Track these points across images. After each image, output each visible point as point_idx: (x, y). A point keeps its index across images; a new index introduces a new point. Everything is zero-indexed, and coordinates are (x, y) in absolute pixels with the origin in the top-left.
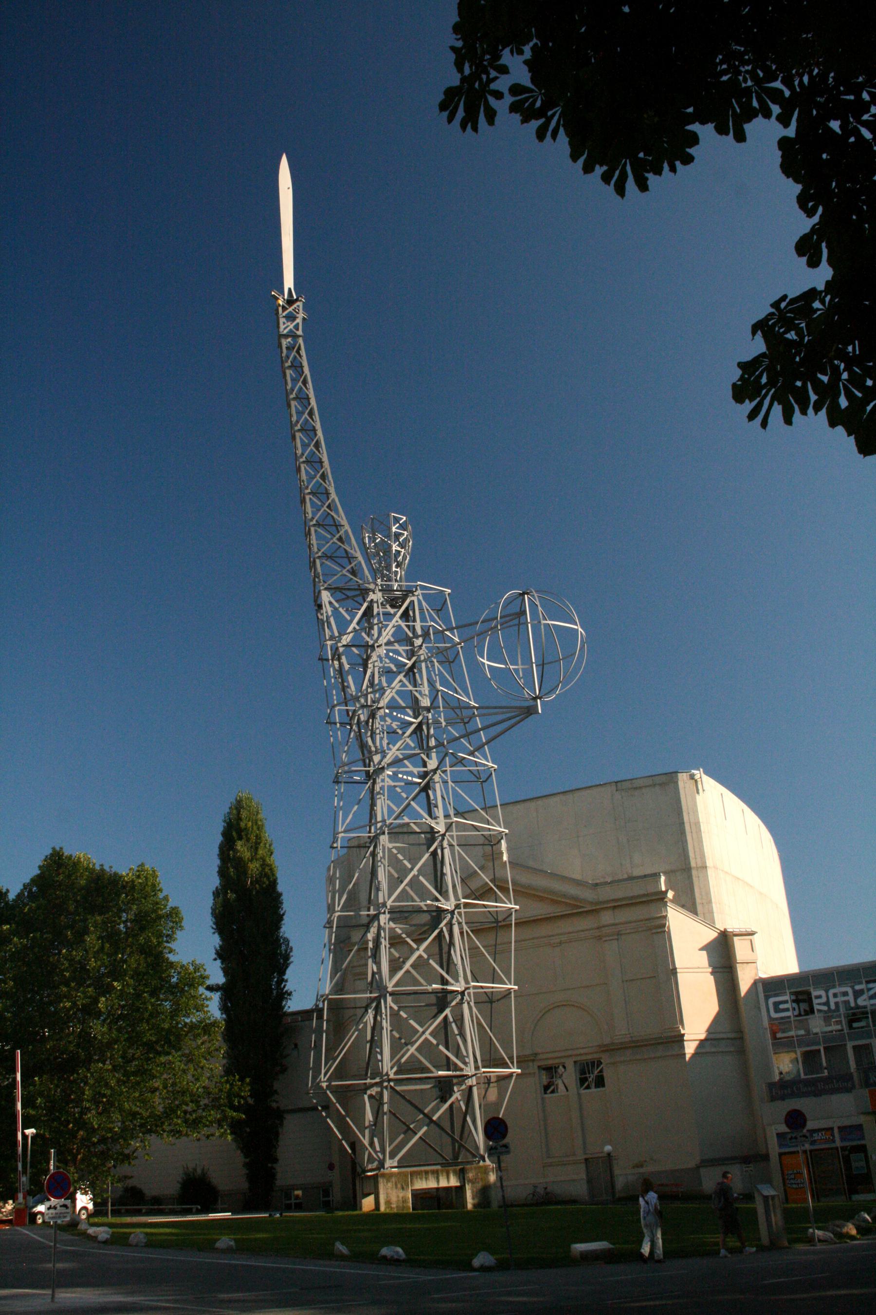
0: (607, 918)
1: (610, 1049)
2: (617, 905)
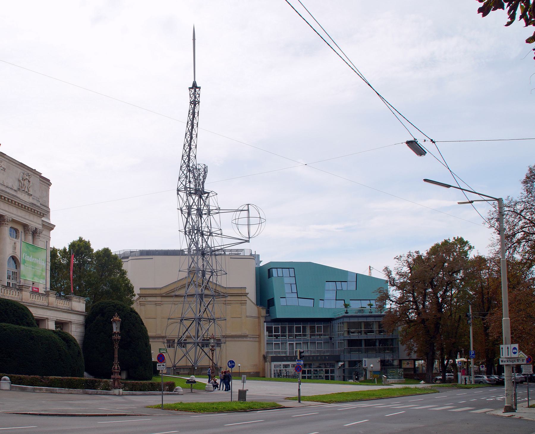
0: (229, 298)
1: (224, 337)
2: (232, 295)
